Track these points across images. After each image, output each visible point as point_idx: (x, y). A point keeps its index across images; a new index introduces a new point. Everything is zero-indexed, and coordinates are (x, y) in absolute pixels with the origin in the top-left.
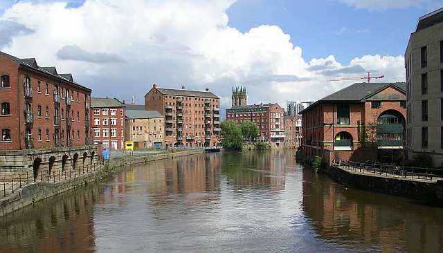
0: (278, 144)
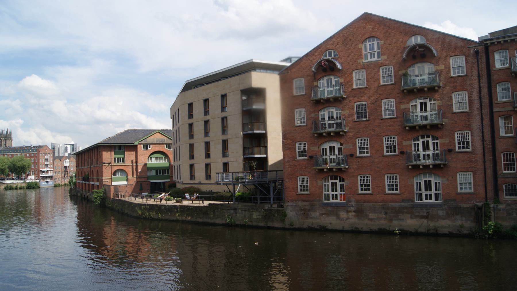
0: (47, 182)
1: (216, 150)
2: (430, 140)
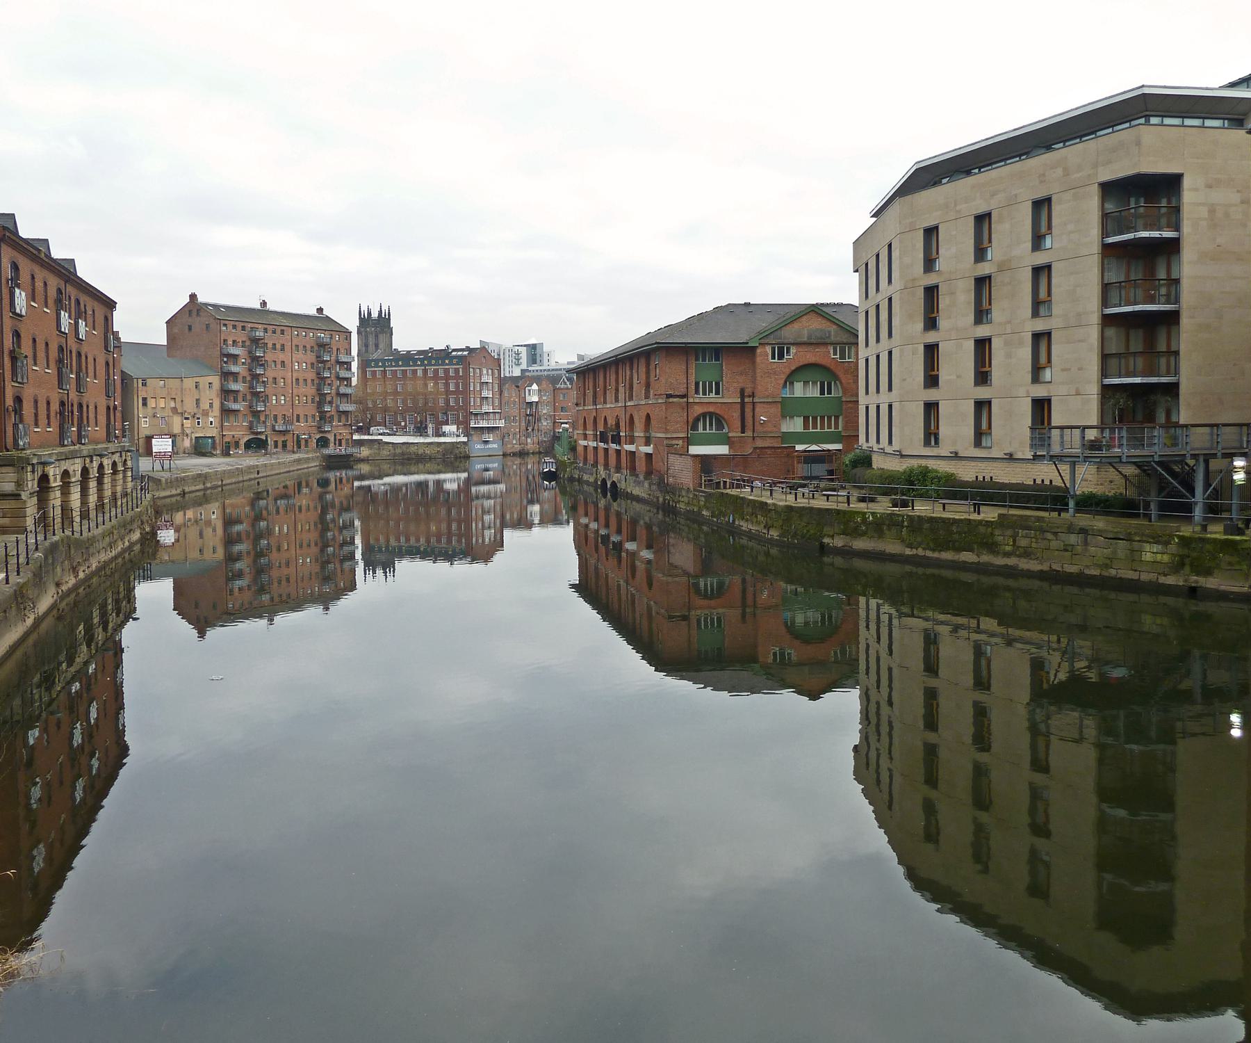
1: (1011, 361)
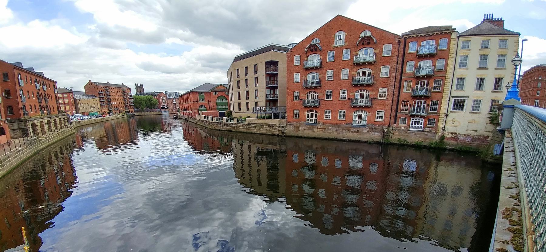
1: (252, 95)
2: (365, 92)
